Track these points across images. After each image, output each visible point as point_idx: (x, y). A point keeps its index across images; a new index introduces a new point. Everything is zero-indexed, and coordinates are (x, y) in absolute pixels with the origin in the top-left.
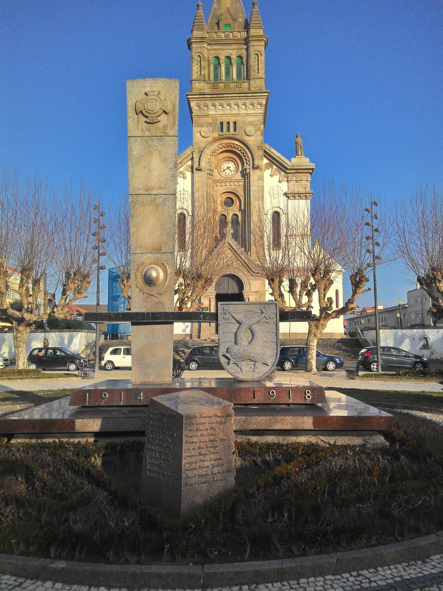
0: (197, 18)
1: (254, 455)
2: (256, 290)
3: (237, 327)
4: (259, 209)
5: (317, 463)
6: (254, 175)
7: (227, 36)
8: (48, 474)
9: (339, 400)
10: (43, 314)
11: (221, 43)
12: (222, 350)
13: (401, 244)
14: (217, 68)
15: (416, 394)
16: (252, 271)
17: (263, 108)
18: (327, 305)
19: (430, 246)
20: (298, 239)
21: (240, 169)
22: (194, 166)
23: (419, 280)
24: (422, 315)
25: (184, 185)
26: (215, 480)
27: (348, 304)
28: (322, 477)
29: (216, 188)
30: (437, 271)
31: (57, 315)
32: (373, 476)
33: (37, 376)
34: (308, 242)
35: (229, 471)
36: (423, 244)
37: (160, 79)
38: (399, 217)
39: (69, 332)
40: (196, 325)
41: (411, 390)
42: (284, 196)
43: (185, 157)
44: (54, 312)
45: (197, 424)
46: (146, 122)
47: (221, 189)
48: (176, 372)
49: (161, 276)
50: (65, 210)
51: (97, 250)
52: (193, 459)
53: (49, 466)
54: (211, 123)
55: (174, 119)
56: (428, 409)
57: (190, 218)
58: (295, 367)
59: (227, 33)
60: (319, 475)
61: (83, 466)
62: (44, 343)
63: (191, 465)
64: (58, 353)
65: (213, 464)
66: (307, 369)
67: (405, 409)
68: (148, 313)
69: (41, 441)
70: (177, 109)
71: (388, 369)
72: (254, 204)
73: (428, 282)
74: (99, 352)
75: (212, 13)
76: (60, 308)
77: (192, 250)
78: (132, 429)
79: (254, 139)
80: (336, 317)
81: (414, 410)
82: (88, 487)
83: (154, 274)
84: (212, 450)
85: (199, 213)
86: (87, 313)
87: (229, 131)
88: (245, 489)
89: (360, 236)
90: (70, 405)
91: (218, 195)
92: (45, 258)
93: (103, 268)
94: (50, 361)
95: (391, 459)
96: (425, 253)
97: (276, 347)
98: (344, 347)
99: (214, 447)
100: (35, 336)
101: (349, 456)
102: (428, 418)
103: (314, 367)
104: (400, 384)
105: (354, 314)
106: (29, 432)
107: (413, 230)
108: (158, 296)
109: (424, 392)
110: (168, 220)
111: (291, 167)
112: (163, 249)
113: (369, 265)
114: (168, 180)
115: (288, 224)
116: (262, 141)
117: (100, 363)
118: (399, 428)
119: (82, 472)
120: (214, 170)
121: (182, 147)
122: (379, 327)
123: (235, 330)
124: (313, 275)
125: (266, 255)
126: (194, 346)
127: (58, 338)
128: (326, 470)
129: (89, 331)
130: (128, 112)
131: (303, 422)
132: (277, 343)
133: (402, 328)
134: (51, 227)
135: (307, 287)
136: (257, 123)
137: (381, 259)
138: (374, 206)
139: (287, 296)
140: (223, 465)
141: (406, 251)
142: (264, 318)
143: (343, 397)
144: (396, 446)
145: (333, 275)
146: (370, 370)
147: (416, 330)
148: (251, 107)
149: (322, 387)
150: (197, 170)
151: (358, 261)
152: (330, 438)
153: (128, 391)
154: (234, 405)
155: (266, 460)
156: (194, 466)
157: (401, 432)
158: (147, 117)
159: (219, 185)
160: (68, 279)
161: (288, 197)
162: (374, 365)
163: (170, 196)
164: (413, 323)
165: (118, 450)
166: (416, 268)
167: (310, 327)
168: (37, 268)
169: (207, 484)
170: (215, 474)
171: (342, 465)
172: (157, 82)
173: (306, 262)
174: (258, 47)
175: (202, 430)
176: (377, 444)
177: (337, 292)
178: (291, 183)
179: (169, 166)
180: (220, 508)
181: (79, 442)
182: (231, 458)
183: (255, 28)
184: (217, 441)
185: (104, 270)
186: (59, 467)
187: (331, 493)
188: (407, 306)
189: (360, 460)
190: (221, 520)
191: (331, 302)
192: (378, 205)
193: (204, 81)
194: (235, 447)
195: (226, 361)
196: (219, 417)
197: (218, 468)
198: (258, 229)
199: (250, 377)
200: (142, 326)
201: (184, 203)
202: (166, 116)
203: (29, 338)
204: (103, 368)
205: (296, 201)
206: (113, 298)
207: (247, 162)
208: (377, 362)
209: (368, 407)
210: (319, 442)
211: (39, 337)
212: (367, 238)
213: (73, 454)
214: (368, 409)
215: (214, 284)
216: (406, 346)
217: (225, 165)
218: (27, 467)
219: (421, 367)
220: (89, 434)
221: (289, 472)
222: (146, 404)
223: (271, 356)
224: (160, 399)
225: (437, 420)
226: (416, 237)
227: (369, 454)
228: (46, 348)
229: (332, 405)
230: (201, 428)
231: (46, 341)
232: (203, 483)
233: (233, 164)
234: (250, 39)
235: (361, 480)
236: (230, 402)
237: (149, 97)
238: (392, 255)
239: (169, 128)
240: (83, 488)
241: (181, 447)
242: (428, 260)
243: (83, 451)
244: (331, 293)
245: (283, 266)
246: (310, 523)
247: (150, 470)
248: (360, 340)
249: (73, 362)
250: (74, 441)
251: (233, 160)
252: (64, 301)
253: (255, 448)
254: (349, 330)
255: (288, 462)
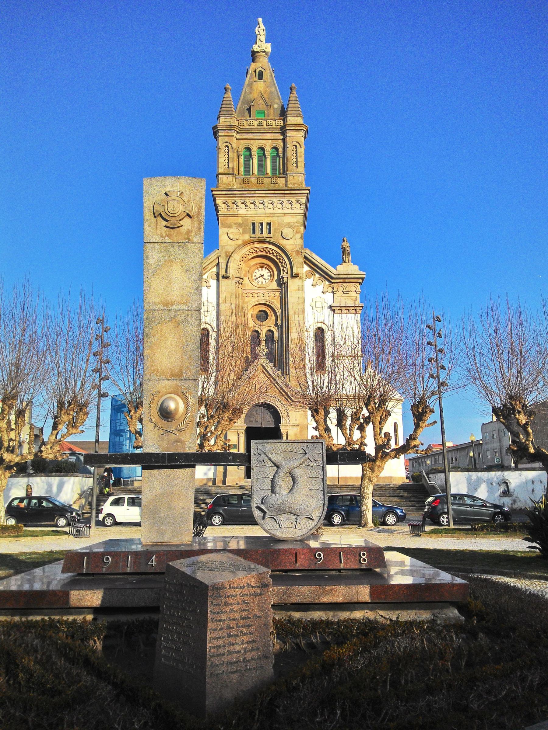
0: (224, 102)
1: (296, 636)
2: (296, 423)
3: (274, 472)
4: (299, 324)
5: (376, 646)
6: (293, 285)
7: (260, 124)
8: (34, 662)
9: (402, 563)
10: (27, 452)
11: (253, 131)
12: (256, 501)
13: (470, 367)
14: (248, 161)
15: (496, 554)
16: (291, 399)
17: (303, 208)
18: (383, 442)
19: (506, 370)
20: (347, 361)
21: (276, 277)
22: (220, 273)
23: (495, 411)
24: (501, 453)
25: (209, 295)
26: (247, 669)
27: (410, 441)
28: (382, 663)
29: (247, 299)
30: (515, 400)
31: (44, 455)
32: (446, 660)
33: (16, 534)
34: (358, 364)
35: (265, 657)
36: (498, 367)
37: (183, 177)
38: (467, 336)
39: (59, 476)
40: (221, 468)
41: (490, 549)
42: (329, 310)
43: (209, 262)
44: (41, 451)
45: (225, 597)
46: (165, 226)
47: (253, 301)
48: (197, 529)
49: (180, 408)
50: (61, 324)
51: (98, 373)
52: (221, 642)
53: (36, 651)
54: (242, 224)
55: (199, 224)
56: (511, 573)
57: (215, 334)
58: (346, 521)
59: (260, 121)
60: (379, 660)
61: (80, 652)
62: (27, 491)
63: (217, 650)
64: (44, 504)
65: (246, 648)
66: (361, 524)
67: (483, 574)
68: (164, 454)
69: (27, 618)
70: (203, 212)
71: (461, 522)
72: (293, 318)
73: (505, 414)
74: (97, 503)
75: (242, 98)
76: (49, 447)
77: (216, 374)
78: (142, 604)
79: (293, 242)
80: (395, 457)
81: (494, 575)
82: (87, 679)
83: (172, 405)
84: (244, 630)
85: (226, 329)
86: (88, 454)
87: (262, 233)
88: (286, 681)
89: (421, 357)
90: (63, 572)
91: (249, 308)
92: (33, 383)
93: (105, 395)
94: (33, 514)
95: (467, 638)
96: (500, 379)
97: (322, 497)
98: (406, 495)
99: (246, 626)
100: (16, 481)
101: (415, 636)
102: (512, 584)
103: (370, 521)
104: (477, 541)
105: (417, 453)
106: (11, 607)
107: (485, 351)
108: (176, 432)
109: (505, 551)
110: (191, 341)
111: (337, 276)
112: (184, 375)
113: (433, 393)
114: (191, 293)
115: (334, 343)
116: (302, 246)
117: (97, 516)
118: (476, 598)
119: (79, 660)
120: (244, 278)
121: (207, 252)
122: (449, 469)
123: (272, 475)
124: (366, 405)
125: (308, 380)
126: (218, 494)
127: (45, 484)
128: (388, 654)
129: (84, 475)
130: (145, 214)
131: (357, 593)
132: (324, 491)
133: (476, 470)
134: (41, 345)
135: (359, 419)
136: (296, 224)
137: (447, 385)
138: (437, 322)
139: (334, 430)
140: (258, 649)
141: (478, 376)
142: (308, 461)
143: (407, 559)
144: (473, 622)
145: (390, 404)
146: (439, 524)
147: (494, 473)
148: (289, 206)
149: (380, 548)
150: (223, 277)
151: (420, 389)
152: (392, 612)
153: (136, 554)
154: (272, 571)
155: (312, 643)
156: (221, 651)
157: (479, 603)
158: (167, 221)
159: (251, 295)
160: (61, 410)
161: (334, 311)
162: (443, 517)
163: (193, 312)
164: (490, 464)
165: (124, 632)
166: (490, 397)
167: (363, 470)
168: (22, 396)
169: (238, 674)
170: (248, 661)
171: (406, 647)
172: (180, 181)
173: (357, 389)
174: (296, 137)
175: (231, 604)
176: (449, 619)
177: (395, 425)
178: (337, 295)
179: (193, 277)
180: (255, 705)
181: (74, 620)
182: (268, 640)
183: (293, 116)
184: (250, 618)
185: (107, 398)
186: (48, 653)
187: (395, 684)
188: (481, 442)
189: (429, 640)
190: (257, 716)
191: (389, 438)
192: (442, 321)
193: (233, 175)
194: (274, 625)
195: (261, 514)
196: (253, 587)
197: (253, 653)
198: (298, 349)
199: (291, 536)
200: (155, 471)
201: (209, 318)
202: (190, 220)
203: (7, 485)
204: (100, 524)
205: (343, 315)
206: (116, 432)
207: (285, 269)
208: (447, 513)
209: (437, 571)
210: (378, 617)
211: (21, 484)
212: (430, 360)
213: (67, 636)
214: (438, 575)
215: (244, 416)
216: (482, 493)
217: (258, 273)
218: (8, 654)
219: (502, 519)
220: (87, 610)
221: (342, 657)
222: (159, 571)
223: (316, 507)
224: (177, 564)
225: (523, 586)
226: (489, 359)
227: (441, 632)
228: (29, 497)
229: (393, 570)
230: (231, 601)
231: (29, 488)
232: (233, 673)
233: (267, 271)
234: (287, 128)
235: (432, 666)
236: (266, 567)
237: (170, 198)
238: (461, 381)
239: (193, 234)
240: (80, 681)
241: (205, 627)
242: (504, 386)
243: (80, 632)
244: (388, 427)
245: (329, 394)
246: (368, 718)
247: (165, 656)
248: (426, 486)
249: (62, 516)
250: (68, 619)
251: (268, 267)
252: (54, 437)
253: (298, 627)
254: (411, 473)
255: (340, 644)
